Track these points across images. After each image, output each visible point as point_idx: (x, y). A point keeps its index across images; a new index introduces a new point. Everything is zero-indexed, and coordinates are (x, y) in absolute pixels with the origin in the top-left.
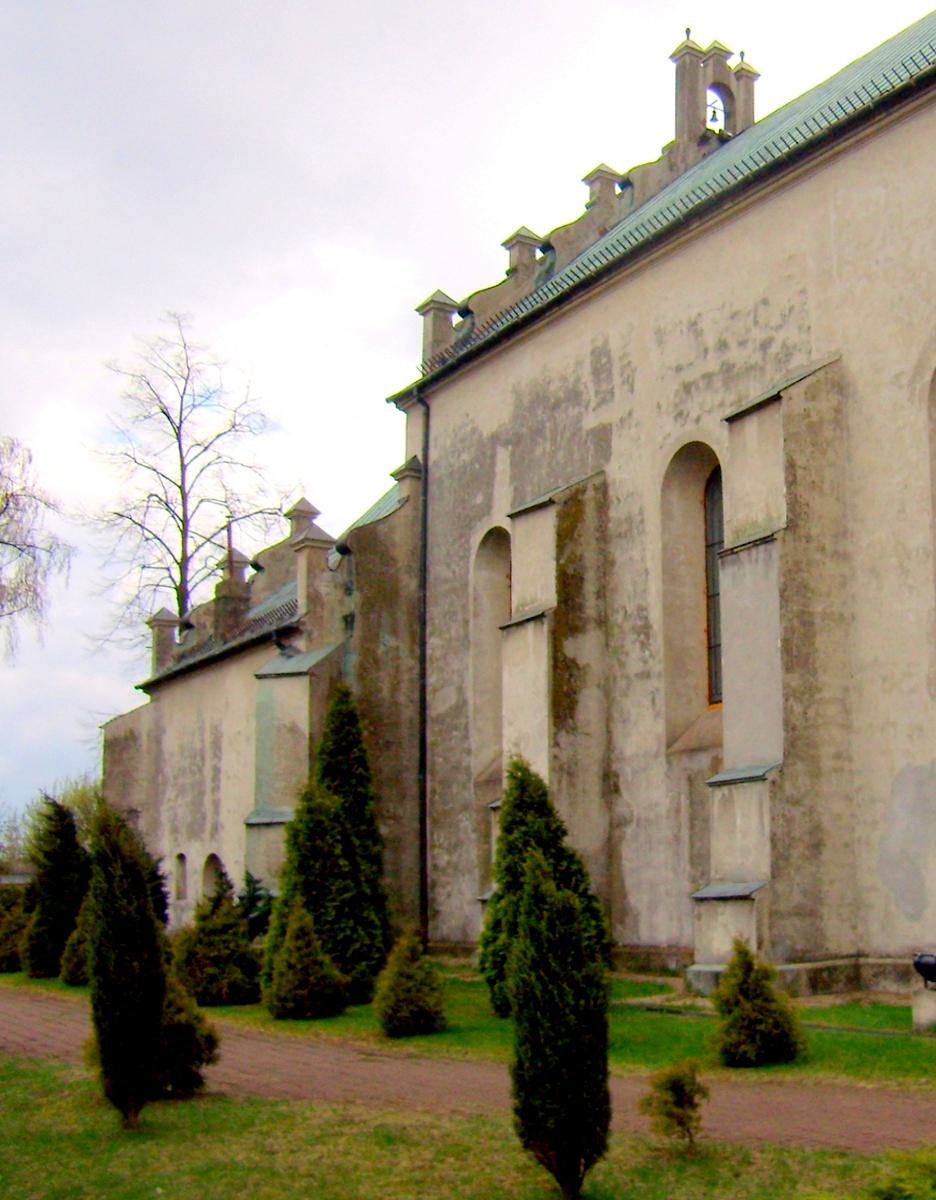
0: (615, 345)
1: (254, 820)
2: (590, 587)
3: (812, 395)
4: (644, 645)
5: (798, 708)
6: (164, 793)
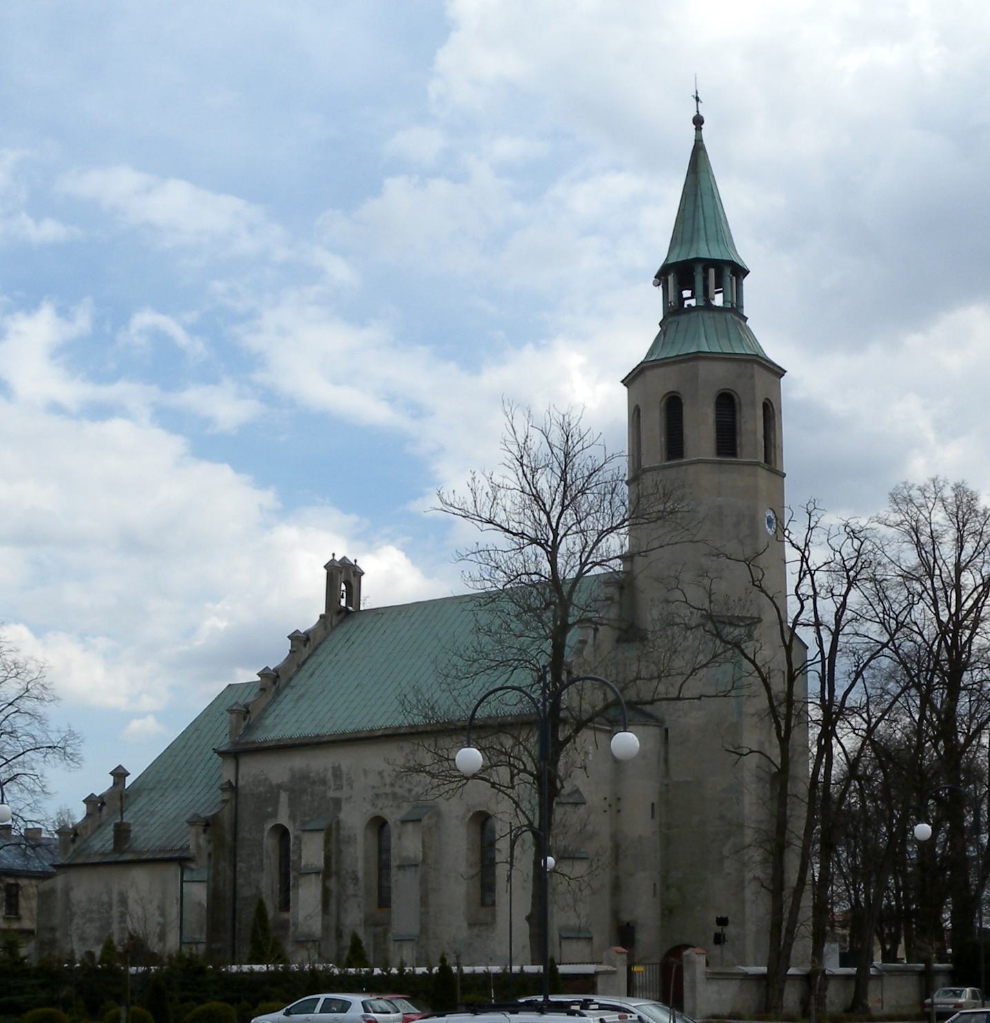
2: (333, 861)
4: (356, 884)
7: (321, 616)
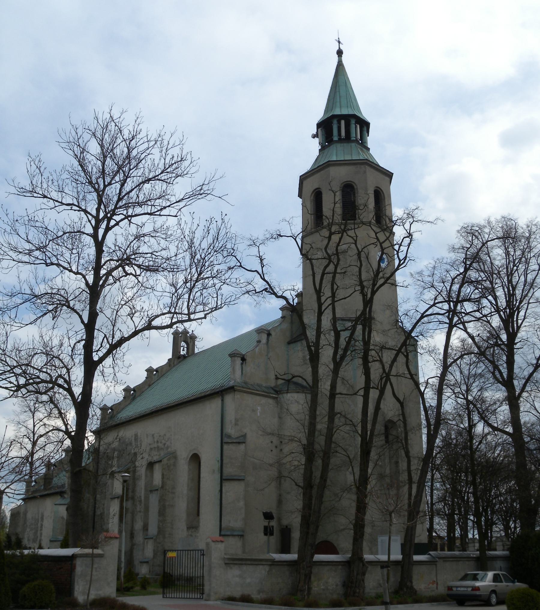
0: (139, 435)
1: (52, 540)
3: (169, 460)
4: (140, 505)
5: (161, 524)
6: (26, 529)
7: (169, 360)
